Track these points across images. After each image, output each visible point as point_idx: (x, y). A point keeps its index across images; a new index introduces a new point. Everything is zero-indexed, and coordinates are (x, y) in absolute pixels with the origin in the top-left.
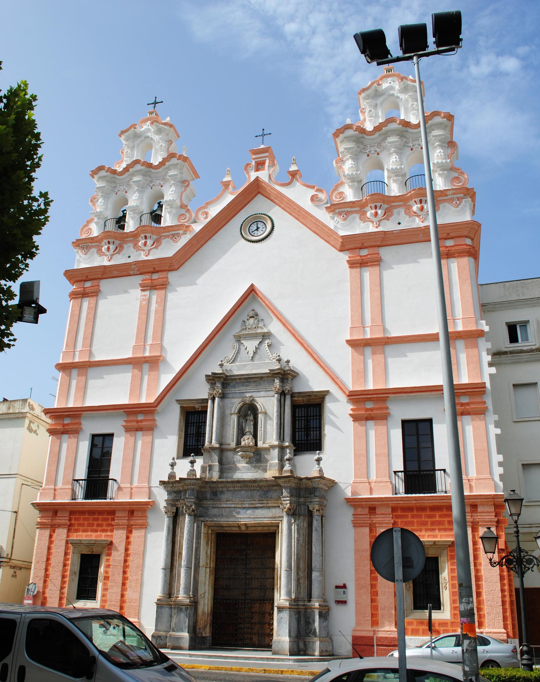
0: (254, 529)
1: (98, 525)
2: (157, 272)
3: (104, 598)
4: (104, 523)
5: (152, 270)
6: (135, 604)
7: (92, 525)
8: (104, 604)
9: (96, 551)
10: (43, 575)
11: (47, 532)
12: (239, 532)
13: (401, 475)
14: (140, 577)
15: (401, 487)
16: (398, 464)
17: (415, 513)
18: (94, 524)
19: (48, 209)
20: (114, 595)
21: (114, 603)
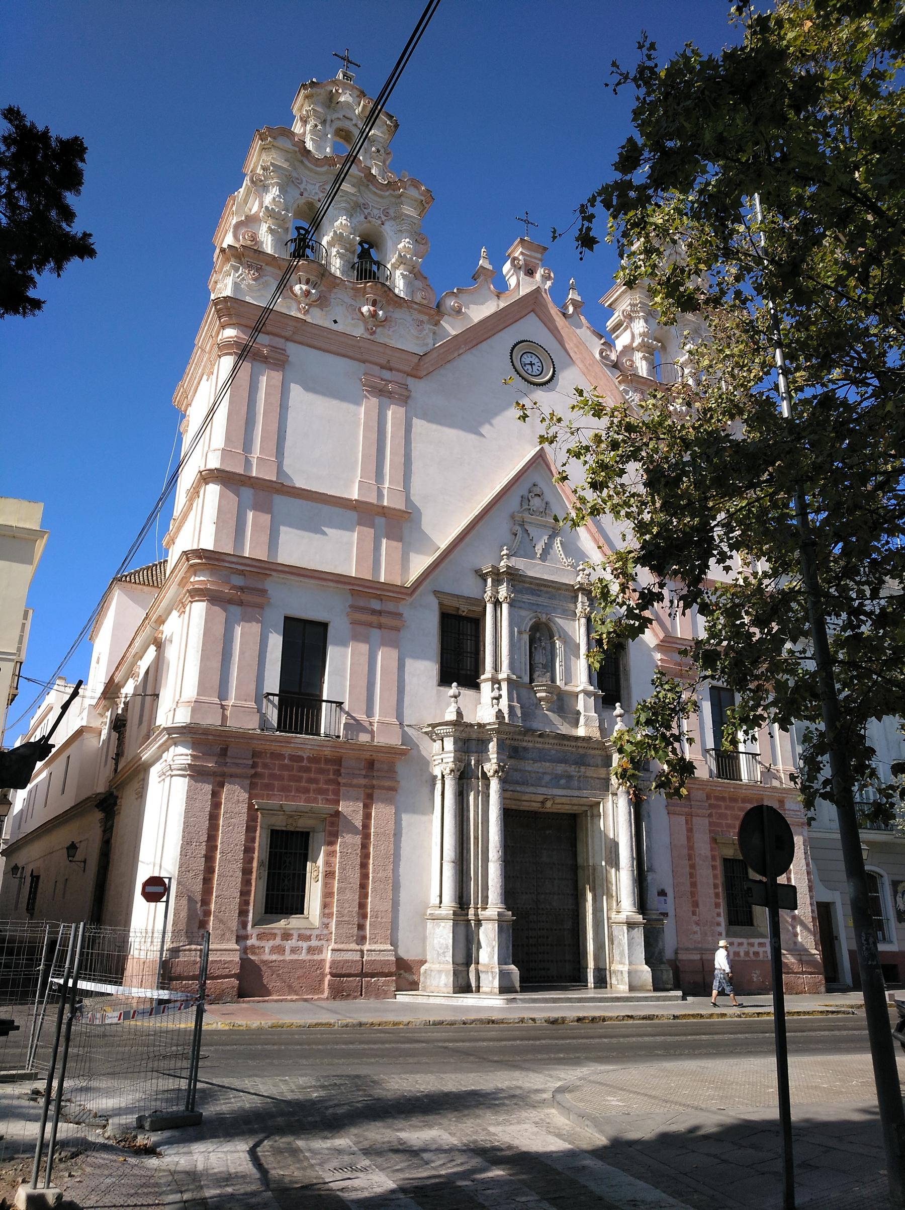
0: (560, 806)
1: (310, 781)
2: (391, 369)
3: (327, 911)
4: (321, 777)
5: (384, 362)
6: (384, 920)
7: (299, 779)
8: (204, 908)
9: (303, 824)
10: (202, 868)
11: (208, 788)
12: (541, 810)
13: (276, 700)
14: (391, 874)
15: (273, 715)
16: (273, 683)
17: (728, 803)
18: (301, 778)
19: (609, 210)
20: (347, 905)
21: (346, 919)
